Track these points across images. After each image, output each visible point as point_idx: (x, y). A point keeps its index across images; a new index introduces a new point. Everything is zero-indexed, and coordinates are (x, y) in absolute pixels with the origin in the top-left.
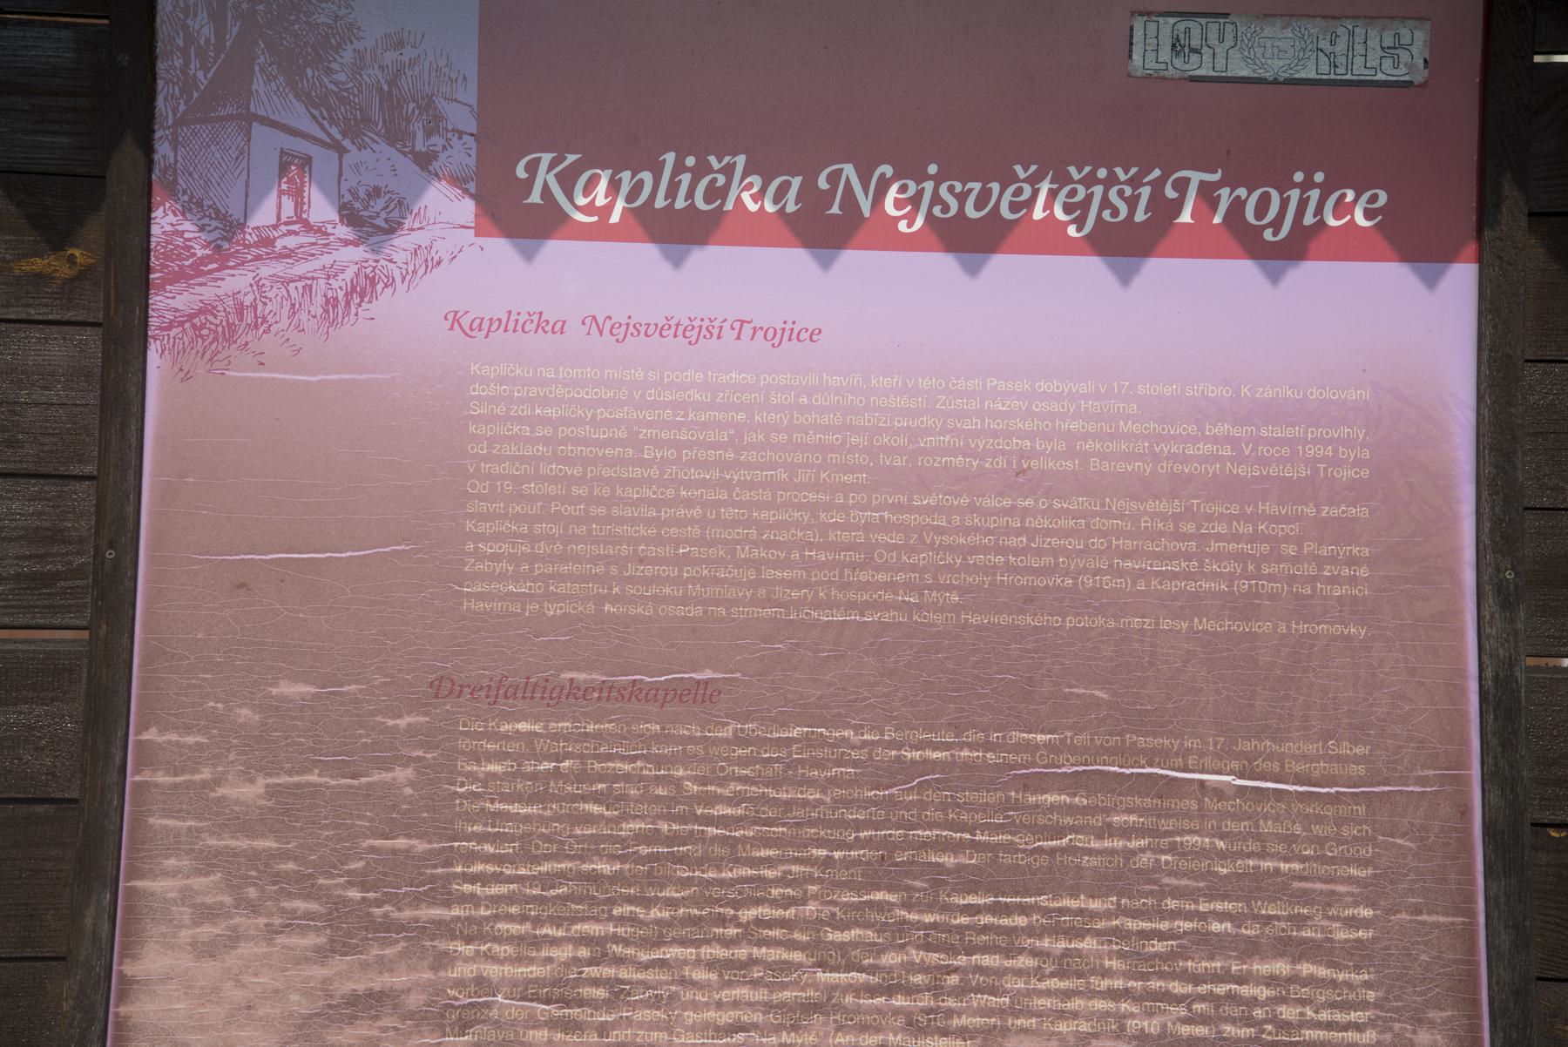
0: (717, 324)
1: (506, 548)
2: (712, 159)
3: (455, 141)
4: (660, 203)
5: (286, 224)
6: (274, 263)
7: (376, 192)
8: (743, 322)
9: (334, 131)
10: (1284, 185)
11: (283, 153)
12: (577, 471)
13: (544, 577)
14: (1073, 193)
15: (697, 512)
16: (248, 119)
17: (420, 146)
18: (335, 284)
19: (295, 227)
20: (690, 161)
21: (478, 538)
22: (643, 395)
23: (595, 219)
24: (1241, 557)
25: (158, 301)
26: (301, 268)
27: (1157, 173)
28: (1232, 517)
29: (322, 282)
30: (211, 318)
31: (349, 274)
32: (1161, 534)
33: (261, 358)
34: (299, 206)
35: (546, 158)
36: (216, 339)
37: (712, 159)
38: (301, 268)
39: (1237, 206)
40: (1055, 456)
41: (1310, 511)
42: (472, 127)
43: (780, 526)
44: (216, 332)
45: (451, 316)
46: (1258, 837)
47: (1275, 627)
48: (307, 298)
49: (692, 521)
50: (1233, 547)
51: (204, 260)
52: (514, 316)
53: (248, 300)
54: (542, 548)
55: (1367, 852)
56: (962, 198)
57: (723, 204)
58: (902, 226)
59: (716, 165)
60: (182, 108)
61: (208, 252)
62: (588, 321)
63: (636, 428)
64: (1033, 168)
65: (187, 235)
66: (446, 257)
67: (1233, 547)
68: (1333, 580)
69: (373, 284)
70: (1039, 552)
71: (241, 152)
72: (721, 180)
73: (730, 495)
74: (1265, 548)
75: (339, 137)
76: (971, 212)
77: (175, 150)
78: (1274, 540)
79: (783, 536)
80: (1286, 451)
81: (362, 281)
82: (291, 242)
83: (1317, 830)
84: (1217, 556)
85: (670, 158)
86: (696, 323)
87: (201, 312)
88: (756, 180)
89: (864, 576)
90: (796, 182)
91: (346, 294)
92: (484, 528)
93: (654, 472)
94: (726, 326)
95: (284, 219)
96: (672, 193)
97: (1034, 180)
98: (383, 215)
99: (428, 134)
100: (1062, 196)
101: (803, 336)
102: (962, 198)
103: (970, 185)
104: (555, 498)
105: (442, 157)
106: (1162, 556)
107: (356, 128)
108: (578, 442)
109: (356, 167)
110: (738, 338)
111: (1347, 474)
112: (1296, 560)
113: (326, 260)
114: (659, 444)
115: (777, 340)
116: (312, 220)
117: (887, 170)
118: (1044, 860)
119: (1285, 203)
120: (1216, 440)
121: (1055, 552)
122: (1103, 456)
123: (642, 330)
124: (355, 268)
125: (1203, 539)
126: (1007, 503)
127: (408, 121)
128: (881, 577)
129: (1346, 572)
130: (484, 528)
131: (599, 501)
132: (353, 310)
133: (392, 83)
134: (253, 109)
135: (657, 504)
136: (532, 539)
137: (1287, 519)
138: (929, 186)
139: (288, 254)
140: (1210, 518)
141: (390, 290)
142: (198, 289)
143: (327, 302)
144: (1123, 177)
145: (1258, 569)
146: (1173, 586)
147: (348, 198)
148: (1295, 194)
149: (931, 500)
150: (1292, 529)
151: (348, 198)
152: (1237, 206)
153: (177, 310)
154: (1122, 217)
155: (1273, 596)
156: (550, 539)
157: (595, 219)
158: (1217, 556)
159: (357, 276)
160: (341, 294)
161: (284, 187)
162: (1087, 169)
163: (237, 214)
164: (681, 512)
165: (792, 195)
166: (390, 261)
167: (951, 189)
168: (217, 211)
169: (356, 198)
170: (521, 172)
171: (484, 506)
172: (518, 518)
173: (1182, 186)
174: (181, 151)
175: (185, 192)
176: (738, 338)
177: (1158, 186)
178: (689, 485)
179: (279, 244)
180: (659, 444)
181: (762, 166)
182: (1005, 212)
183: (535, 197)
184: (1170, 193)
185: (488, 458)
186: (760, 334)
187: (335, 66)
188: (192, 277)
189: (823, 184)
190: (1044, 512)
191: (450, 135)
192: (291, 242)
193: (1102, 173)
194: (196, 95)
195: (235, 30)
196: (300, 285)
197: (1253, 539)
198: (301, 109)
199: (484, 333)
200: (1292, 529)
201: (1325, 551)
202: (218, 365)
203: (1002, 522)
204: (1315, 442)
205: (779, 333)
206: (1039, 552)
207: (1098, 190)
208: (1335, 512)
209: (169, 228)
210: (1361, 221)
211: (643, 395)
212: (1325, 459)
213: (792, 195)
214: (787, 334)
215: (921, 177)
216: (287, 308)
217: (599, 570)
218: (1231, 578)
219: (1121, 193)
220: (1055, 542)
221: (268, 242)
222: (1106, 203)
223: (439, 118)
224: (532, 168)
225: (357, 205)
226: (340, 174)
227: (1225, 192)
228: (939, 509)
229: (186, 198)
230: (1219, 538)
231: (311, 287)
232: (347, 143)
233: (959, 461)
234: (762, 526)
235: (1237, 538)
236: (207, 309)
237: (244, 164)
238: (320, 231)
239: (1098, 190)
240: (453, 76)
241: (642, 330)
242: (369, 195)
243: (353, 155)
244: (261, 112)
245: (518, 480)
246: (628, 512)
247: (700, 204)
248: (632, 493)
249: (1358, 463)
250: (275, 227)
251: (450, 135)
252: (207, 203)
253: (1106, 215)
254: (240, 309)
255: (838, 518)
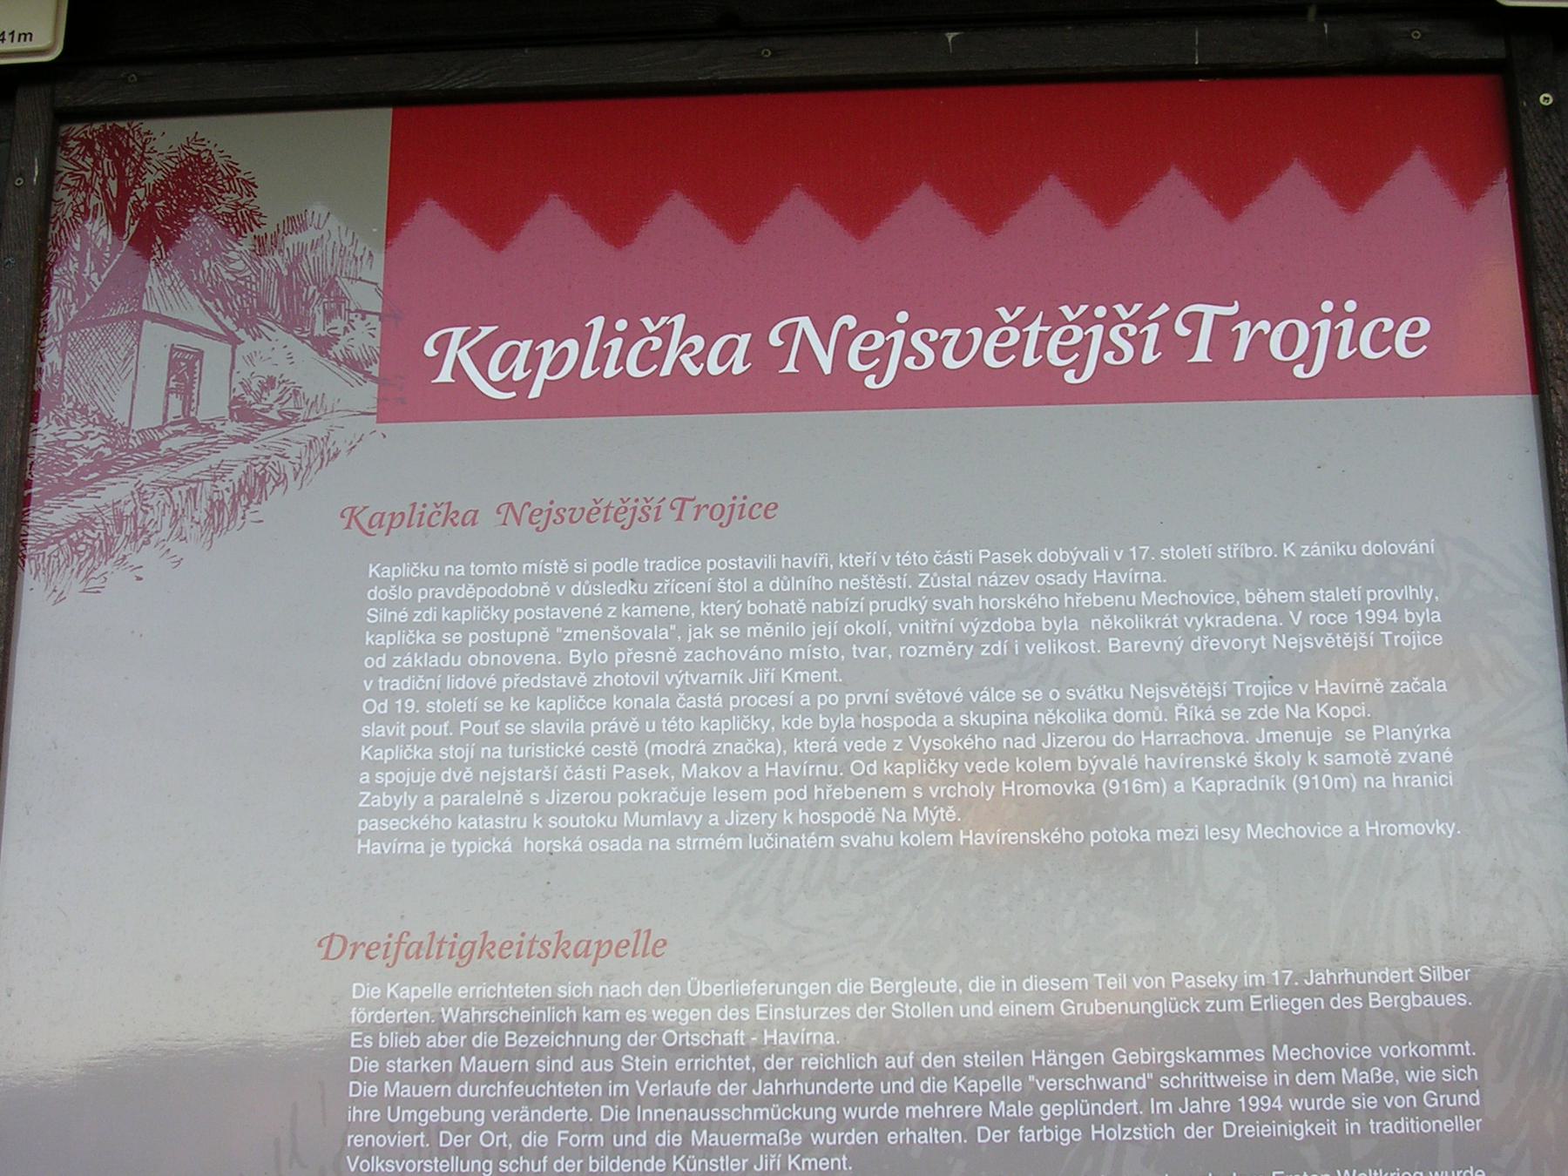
0: (653, 504)
1: (407, 778)
2: (647, 321)
3: (358, 322)
4: (587, 372)
5: (172, 424)
6: (157, 468)
7: (271, 382)
8: (684, 500)
9: (229, 323)
10: (1312, 316)
11: (173, 349)
12: (490, 682)
13: (452, 812)
14: (1068, 335)
15: (633, 725)
16: (139, 317)
17: (319, 331)
18: (221, 485)
19: (182, 427)
20: (621, 325)
21: (375, 766)
22: (568, 590)
23: (513, 394)
24: (1298, 748)
25: (36, 516)
26: (186, 471)
27: (1164, 309)
28: (1285, 699)
29: (208, 484)
30: (88, 532)
31: (237, 474)
32: (1199, 726)
33: (139, 573)
34: (187, 406)
35: (458, 332)
36: (92, 555)
37: (647, 321)
38: (186, 471)
39: (1260, 341)
40: (1067, 637)
41: (1377, 686)
42: (376, 305)
43: (733, 736)
44: (93, 546)
45: (347, 514)
46: (1339, 1089)
47: (1346, 832)
48: (191, 504)
49: (626, 737)
50: (1287, 737)
51: (85, 470)
52: (419, 509)
53: (128, 510)
54: (449, 775)
55: (1474, 1099)
56: (938, 347)
57: (659, 369)
58: (870, 382)
59: (651, 328)
60: (74, 312)
61: (89, 460)
62: (503, 509)
63: (559, 630)
64: (1020, 310)
65: (69, 444)
66: (344, 448)
67: (1287, 737)
68: (1411, 769)
69: (263, 483)
70: (1053, 754)
71: (131, 352)
72: (657, 343)
73: (673, 703)
74: (1327, 735)
75: (233, 328)
76: (950, 362)
77: (63, 357)
78: (1335, 725)
79: (740, 749)
80: (1342, 618)
81: (251, 478)
82: (176, 443)
83: (1412, 1076)
84: (1271, 748)
85: (598, 323)
86: (630, 505)
87: (78, 526)
88: (698, 342)
89: (837, 794)
90: (744, 340)
91: (233, 497)
92: (382, 755)
93: (582, 681)
94: (665, 506)
95: (170, 419)
96: (600, 360)
97: (1021, 323)
98: (277, 406)
99: (329, 316)
100: (1054, 342)
101: (757, 512)
102: (938, 347)
103: (946, 333)
104: (466, 715)
105: (343, 340)
106: (1201, 751)
107: (249, 321)
108: (490, 649)
109: (250, 359)
110: (679, 519)
111: (1414, 642)
112: (1365, 747)
113: (214, 460)
114: (586, 646)
115: (725, 520)
116: (200, 418)
117: (850, 321)
118: (1075, 1135)
119: (1314, 336)
120: (1257, 609)
121: (1071, 754)
122: (1123, 635)
123: (567, 515)
124: (243, 467)
125: (1248, 728)
126: (1010, 696)
127: (307, 304)
128: (860, 793)
129: (1425, 758)
130: (382, 755)
131: (515, 717)
132: (240, 514)
133: (292, 267)
134: (145, 307)
135: (588, 717)
136: (438, 765)
137: (1352, 699)
138: (899, 336)
139: (173, 456)
140: (1257, 702)
141: (281, 488)
142: (77, 502)
143: (213, 504)
144: (1125, 315)
145: (1320, 759)
146: (1218, 787)
147: (240, 391)
148: (1325, 326)
149: (918, 697)
150: (1359, 711)
151: (240, 391)
152: (1260, 341)
153: (54, 526)
154: (1126, 360)
155: (1343, 792)
156: (458, 765)
157: (513, 394)
158: (1271, 748)
159: (246, 474)
160: (227, 496)
161: (173, 385)
162: (1083, 308)
163: (122, 418)
164: (615, 727)
165: (740, 354)
166: (282, 456)
167: (925, 338)
168: (101, 416)
169: (249, 392)
170: (430, 350)
171: (381, 731)
172: (422, 742)
173: (1194, 321)
174: (69, 357)
175: (70, 399)
176: (679, 519)
177: (1166, 323)
178: (623, 692)
179: (164, 446)
180: (586, 646)
181: (705, 324)
182: (990, 360)
183: (445, 376)
184: (1182, 330)
185: (388, 673)
186: (705, 513)
187: (233, 255)
188: (71, 489)
189: (775, 340)
190: (1056, 705)
191: (352, 316)
192: (176, 443)
193: (1100, 312)
194: (88, 298)
195: (132, 229)
196: (184, 489)
197: (1312, 724)
198: (194, 300)
199: (384, 530)
200: (1359, 711)
201: (1398, 735)
202: (92, 583)
203: (1005, 720)
204: (1376, 605)
205: (728, 511)
206: (1053, 754)
207: (1097, 330)
208: (1408, 688)
209: (51, 438)
210: (1403, 352)
211: (568, 590)
212: (1389, 625)
213: (740, 354)
214: (737, 510)
215: (889, 326)
216: (169, 515)
217: (517, 798)
218: (1288, 773)
219: (1124, 332)
220: (1071, 741)
221: (153, 445)
222: (1107, 344)
223: (341, 299)
224: (443, 345)
225: (249, 398)
226: (233, 367)
227: (1244, 326)
228: (927, 708)
229: (71, 405)
230: (1271, 725)
231: (195, 490)
232: (241, 334)
233: (950, 650)
234: (711, 738)
235: (1291, 724)
236: (85, 522)
237: (132, 365)
238: (208, 429)
239: (1097, 330)
240: (358, 255)
241: (567, 515)
242: (264, 388)
243: (248, 345)
244: (154, 309)
245: (421, 697)
246: (551, 728)
247: (633, 370)
248: (555, 706)
249: (1429, 628)
250: (160, 429)
251: (352, 316)
252: (91, 408)
253: (1109, 357)
254: (119, 519)
255: (804, 723)
